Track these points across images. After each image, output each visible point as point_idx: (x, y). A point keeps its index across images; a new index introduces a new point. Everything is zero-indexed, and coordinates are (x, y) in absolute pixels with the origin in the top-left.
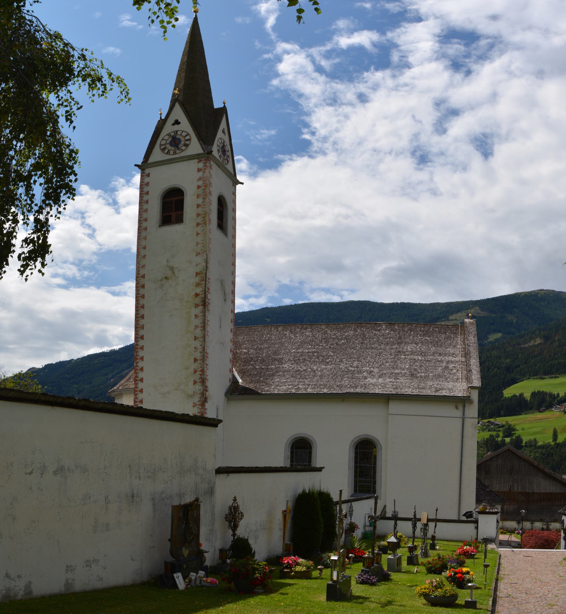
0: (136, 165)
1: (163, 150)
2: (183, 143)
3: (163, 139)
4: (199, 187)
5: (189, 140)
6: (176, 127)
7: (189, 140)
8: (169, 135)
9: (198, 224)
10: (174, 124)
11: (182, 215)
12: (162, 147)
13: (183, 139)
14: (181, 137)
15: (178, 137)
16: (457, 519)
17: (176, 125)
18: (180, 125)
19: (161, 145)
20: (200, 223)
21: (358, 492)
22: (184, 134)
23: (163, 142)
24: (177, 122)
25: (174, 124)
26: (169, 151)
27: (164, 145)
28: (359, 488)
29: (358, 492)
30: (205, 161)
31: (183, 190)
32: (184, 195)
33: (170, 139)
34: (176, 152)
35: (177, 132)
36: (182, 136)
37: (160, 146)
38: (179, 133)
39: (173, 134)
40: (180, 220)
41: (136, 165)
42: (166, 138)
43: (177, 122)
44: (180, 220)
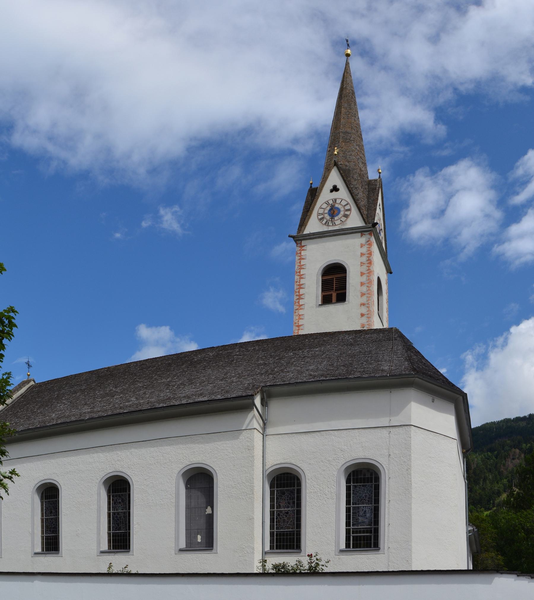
0: (290, 236)
1: (321, 220)
2: (342, 213)
3: (321, 208)
4: (362, 284)
5: (349, 210)
6: (335, 195)
7: (349, 210)
8: (327, 203)
9: (362, 315)
10: (332, 191)
11: (345, 294)
12: (320, 217)
13: (342, 209)
14: (340, 207)
15: (336, 206)
16: (466, 569)
17: (334, 192)
18: (339, 191)
19: (319, 214)
20: (365, 314)
21: (275, 549)
22: (344, 203)
23: (321, 211)
24: (335, 189)
25: (332, 191)
26: (327, 221)
27: (322, 214)
28: (353, 541)
29: (275, 549)
30: (369, 246)
31: (346, 266)
32: (346, 273)
33: (329, 208)
34: (335, 223)
35: (336, 200)
36: (341, 205)
37: (318, 216)
38: (338, 201)
39: (331, 202)
40: (342, 298)
41: (290, 236)
42: (325, 206)
43: (335, 189)
44: (342, 298)
